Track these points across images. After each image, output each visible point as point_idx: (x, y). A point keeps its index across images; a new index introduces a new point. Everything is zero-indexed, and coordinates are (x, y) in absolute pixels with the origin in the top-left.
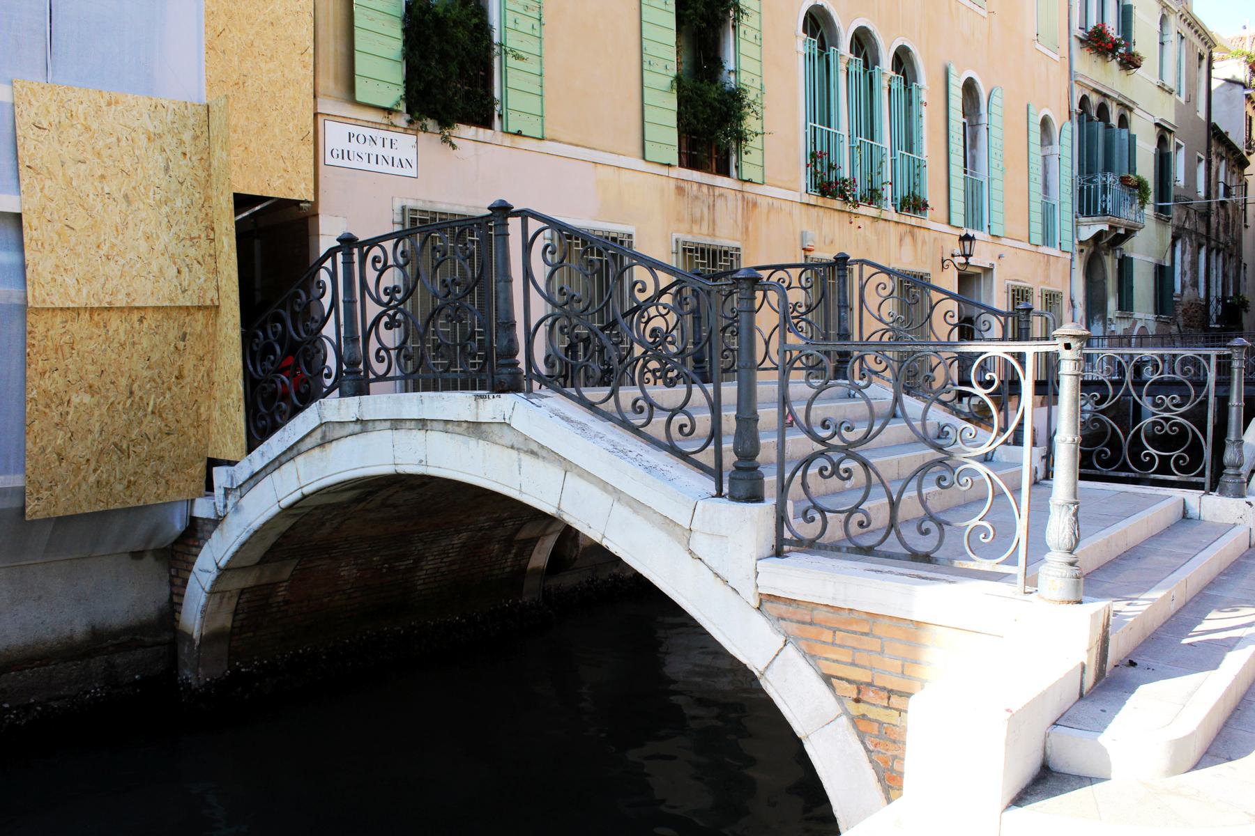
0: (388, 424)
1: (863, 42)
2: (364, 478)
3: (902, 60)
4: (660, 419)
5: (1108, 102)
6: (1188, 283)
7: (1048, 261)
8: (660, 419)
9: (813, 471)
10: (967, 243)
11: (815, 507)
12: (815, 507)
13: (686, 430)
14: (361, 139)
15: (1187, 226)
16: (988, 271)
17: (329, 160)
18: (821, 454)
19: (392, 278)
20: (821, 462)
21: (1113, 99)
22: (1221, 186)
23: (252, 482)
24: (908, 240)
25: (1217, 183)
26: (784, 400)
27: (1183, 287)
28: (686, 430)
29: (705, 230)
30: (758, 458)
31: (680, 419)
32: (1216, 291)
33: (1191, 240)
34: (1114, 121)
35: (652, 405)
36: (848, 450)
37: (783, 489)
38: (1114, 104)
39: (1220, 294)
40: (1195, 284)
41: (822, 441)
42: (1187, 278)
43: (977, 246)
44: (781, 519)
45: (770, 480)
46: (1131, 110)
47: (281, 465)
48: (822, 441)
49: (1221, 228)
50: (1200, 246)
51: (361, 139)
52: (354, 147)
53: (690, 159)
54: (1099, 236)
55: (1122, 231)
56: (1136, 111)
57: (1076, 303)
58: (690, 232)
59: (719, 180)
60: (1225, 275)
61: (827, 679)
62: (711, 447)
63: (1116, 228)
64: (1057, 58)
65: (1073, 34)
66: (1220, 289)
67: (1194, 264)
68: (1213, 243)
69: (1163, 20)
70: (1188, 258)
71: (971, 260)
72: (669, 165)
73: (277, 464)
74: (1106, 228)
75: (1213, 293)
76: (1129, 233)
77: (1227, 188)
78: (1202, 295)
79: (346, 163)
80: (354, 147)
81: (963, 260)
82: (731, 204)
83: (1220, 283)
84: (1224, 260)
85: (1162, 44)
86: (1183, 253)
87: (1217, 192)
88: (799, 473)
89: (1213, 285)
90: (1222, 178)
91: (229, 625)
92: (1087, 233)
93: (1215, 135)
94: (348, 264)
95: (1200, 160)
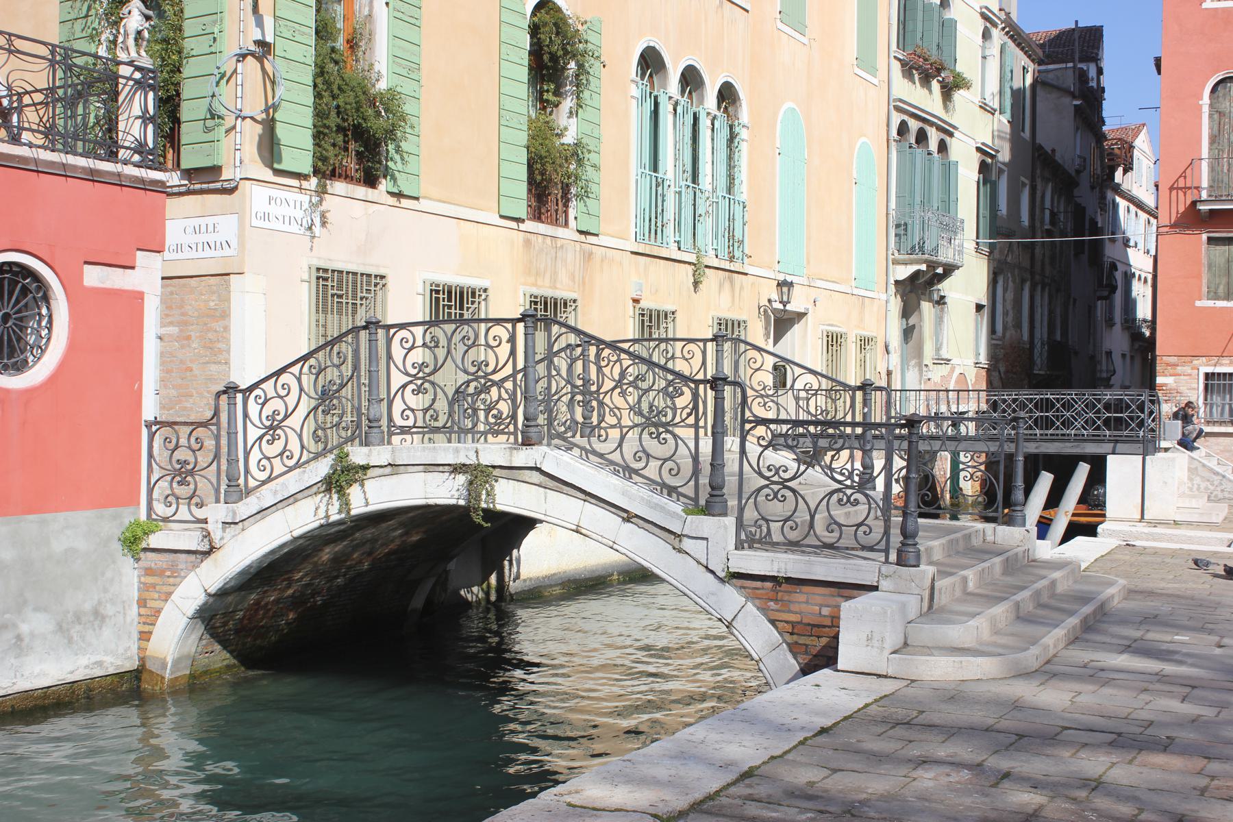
0: (421, 468)
1: (691, 79)
2: (437, 505)
3: (727, 95)
4: (655, 464)
5: (928, 129)
6: (1010, 324)
7: (863, 303)
8: (655, 464)
9: (761, 498)
10: (785, 289)
11: (763, 518)
12: (763, 518)
13: (673, 472)
14: (278, 201)
15: (1009, 259)
16: (801, 316)
17: (255, 223)
18: (767, 486)
19: (418, 356)
20: (766, 491)
21: (932, 124)
22: (1047, 213)
23: (258, 516)
24: (727, 285)
25: (1043, 209)
26: (743, 451)
27: (1005, 328)
28: (673, 472)
29: (547, 282)
30: (725, 491)
31: (669, 464)
32: (1041, 332)
33: (1013, 275)
34: (933, 145)
35: (648, 455)
36: (783, 483)
37: (741, 510)
38: (934, 129)
39: (1045, 336)
40: (1018, 325)
41: (767, 478)
42: (1010, 319)
43: (796, 290)
44: (740, 524)
45: (732, 503)
46: (951, 135)
47: (296, 501)
48: (767, 478)
49: (1047, 261)
50: (1023, 281)
51: (278, 201)
52: (274, 210)
53: (537, 214)
54: (915, 276)
55: (940, 270)
56: (956, 134)
57: (891, 348)
58: (535, 285)
59: (560, 232)
60: (1051, 312)
61: (773, 622)
62: (692, 483)
63: (934, 268)
64: (875, 81)
65: (892, 55)
66: (1045, 330)
67: (1017, 303)
68: (1037, 277)
69: (986, 35)
70: (1010, 295)
71: (788, 307)
72: (518, 220)
73: (292, 500)
74: (924, 267)
75: (1038, 335)
76: (949, 269)
77: (1053, 214)
78: (1026, 337)
79: (266, 224)
80: (274, 210)
81: (781, 307)
82: (570, 256)
83: (1046, 323)
84: (1050, 297)
85: (984, 58)
86: (1005, 290)
87: (1042, 222)
88: (752, 500)
89: (1037, 325)
90: (1048, 204)
91: (193, 650)
92: (904, 272)
93: (1040, 155)
94: (372, 341)
95: (1024, 185)
